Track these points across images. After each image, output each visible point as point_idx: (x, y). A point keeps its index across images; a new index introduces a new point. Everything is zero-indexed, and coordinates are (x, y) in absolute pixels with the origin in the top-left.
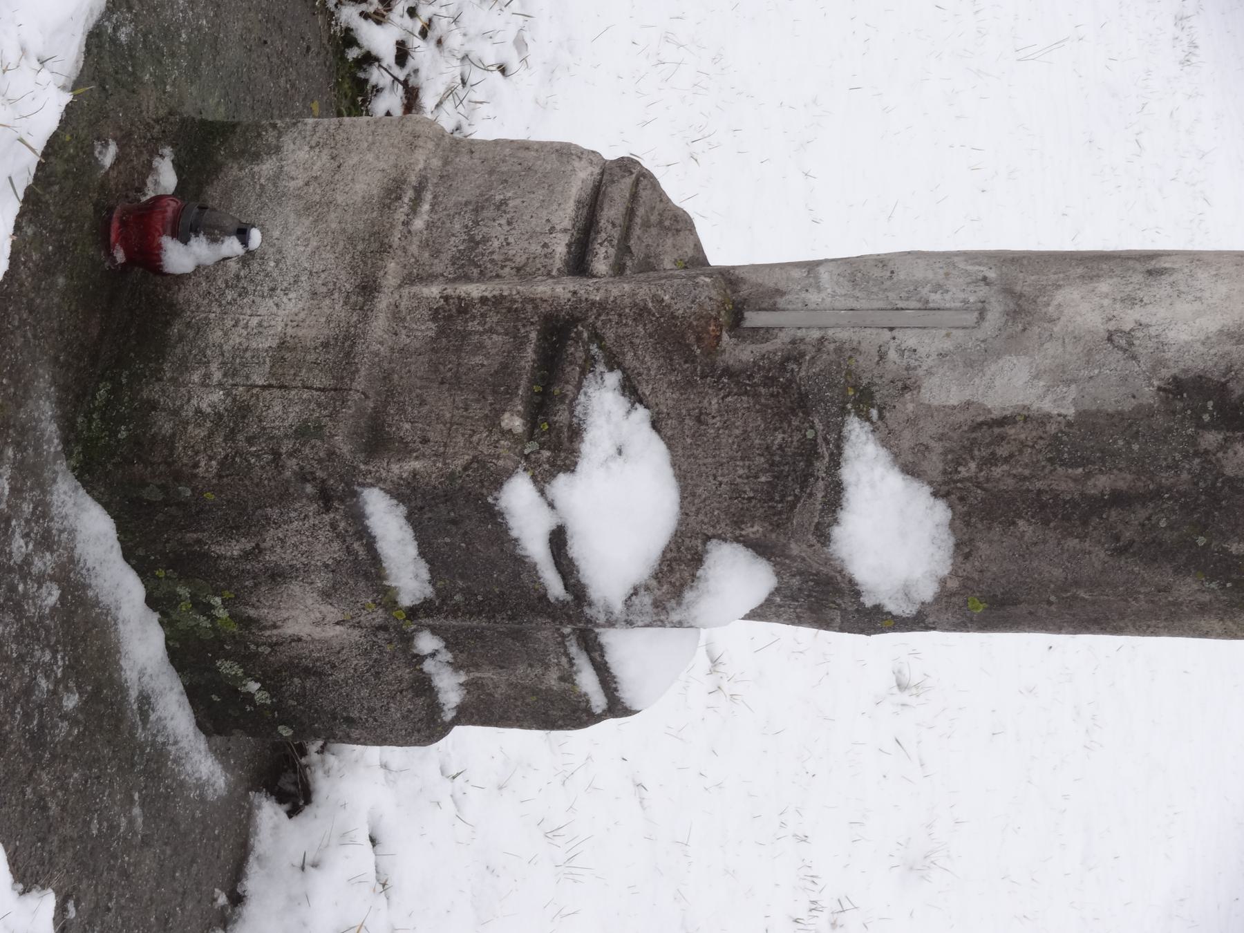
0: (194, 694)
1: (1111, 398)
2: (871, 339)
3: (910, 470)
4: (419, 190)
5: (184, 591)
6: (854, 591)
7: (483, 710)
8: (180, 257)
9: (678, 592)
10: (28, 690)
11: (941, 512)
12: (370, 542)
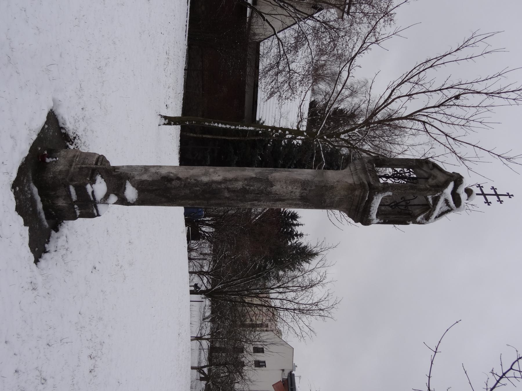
0: (45, 214)
1: (155, 178)
2: (129, 172)
3: (133, 186)
4: (77, 156)
5: (46, 199)
6: (126, 200)
7: (82, 216)
8: (48, 160)
9: (106, 199)
10: (26, 206)
11: (137, 191)
12: (70, 192)
